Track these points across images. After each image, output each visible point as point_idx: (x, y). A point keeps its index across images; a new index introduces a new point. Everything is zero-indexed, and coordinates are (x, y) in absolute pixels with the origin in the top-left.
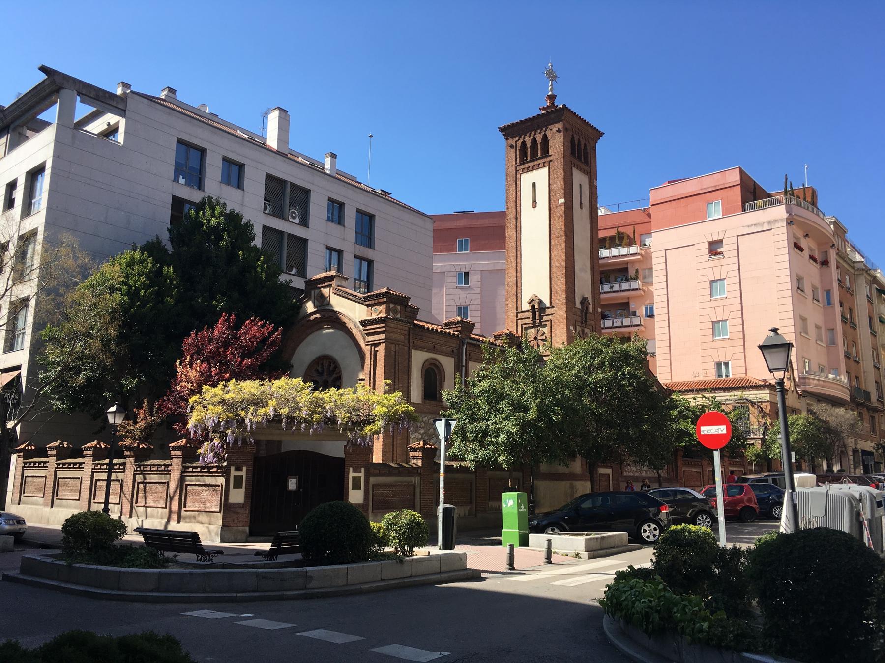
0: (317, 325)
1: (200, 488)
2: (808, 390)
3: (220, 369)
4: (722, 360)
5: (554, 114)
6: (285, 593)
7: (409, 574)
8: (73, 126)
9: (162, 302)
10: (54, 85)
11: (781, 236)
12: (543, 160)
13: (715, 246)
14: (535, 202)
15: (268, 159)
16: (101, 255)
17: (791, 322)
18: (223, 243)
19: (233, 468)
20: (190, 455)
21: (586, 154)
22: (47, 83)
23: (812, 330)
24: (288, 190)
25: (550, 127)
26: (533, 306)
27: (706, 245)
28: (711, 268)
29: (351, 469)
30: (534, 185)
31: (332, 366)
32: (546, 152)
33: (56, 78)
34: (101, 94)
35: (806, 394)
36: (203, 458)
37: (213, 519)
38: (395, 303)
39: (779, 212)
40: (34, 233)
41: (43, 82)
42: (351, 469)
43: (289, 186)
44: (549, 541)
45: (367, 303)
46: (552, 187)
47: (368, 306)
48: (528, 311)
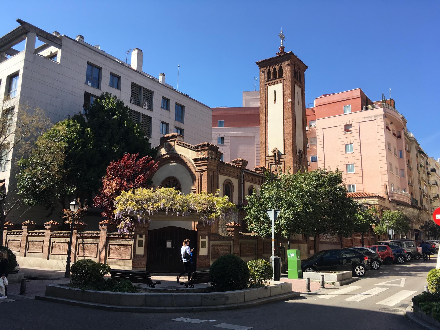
0: (167, 161)
1: (118, 246)
2: (394, 199)
3: (131, 181)
4: (351, 184)
5: (284, 56)
6: (219, 307)
7: (269, 295)
8: (34, 52)
9: (86, 147)
10: (24, 30)
11: (381, 123)
12: (280, 79)
13: (348, 127)
14: (275, 100)
15: (133, 75)
16: (55, 122)
17: (386, 165)
18: (115, 117)
19: (138, 236)
20: (112, 229)
21: (300, 77)
22: (20, 28)
23: (394, 169)
24: (142, 91)
25: (283, 63)
26: (275, 154)
27: (343, 127)
28: (346, 138)
29: (201, 237)
30: (275, 92)
31: (175, 183)
32: (281, 75)
33: (26, 26)
34: (49, 36)
35: (393, 201)
36: (121, 230)
37: (126, 264)
38: (212, 150)
39: (380, 111)
40: (13, 108)
41: (18, 28)
42: (201, 237)
43: (143, 89)
44: (323, 276)
45: (197, 149)
46: (285, 93)
47: (197, 151)
48: (272, 156)
